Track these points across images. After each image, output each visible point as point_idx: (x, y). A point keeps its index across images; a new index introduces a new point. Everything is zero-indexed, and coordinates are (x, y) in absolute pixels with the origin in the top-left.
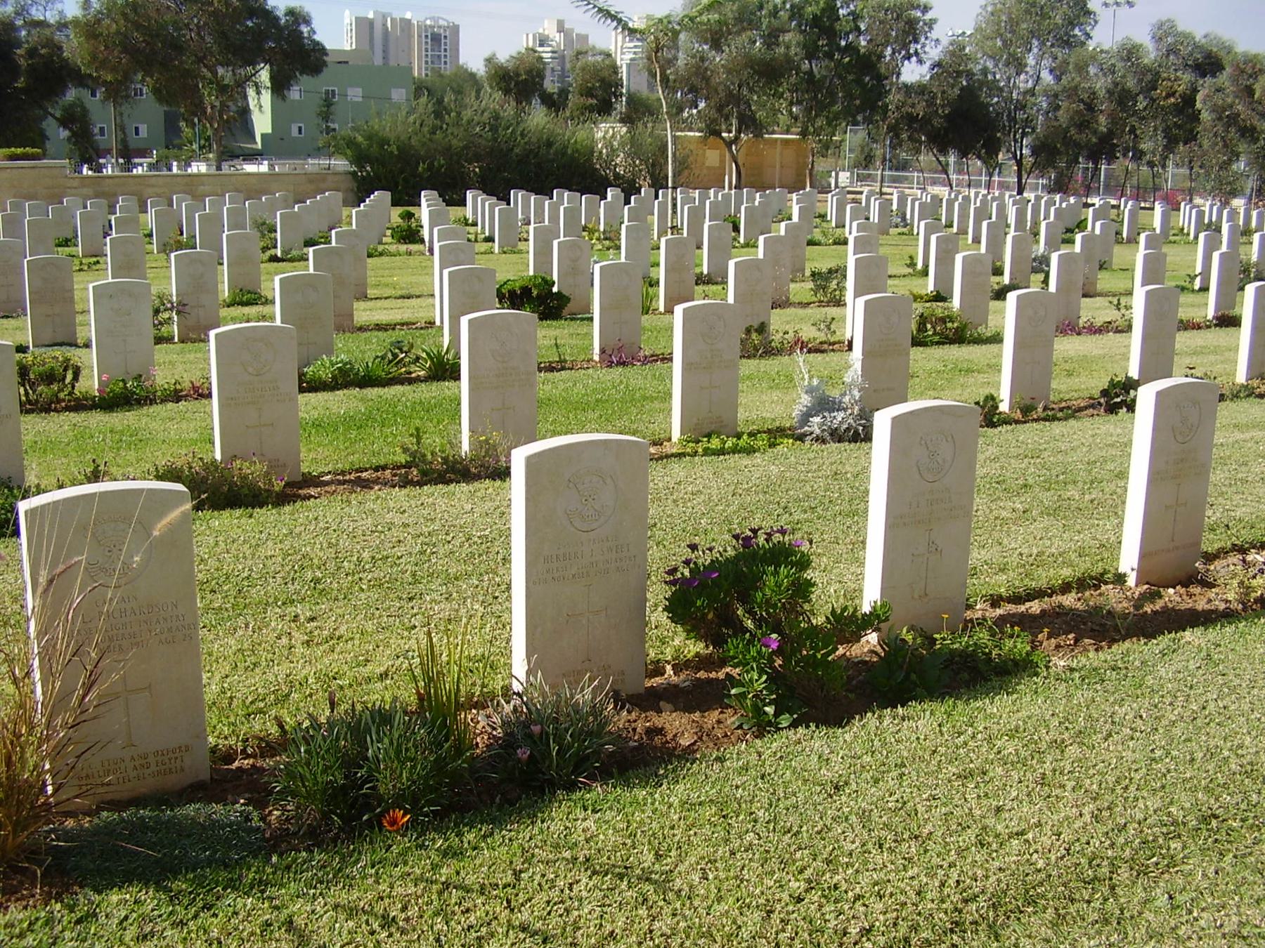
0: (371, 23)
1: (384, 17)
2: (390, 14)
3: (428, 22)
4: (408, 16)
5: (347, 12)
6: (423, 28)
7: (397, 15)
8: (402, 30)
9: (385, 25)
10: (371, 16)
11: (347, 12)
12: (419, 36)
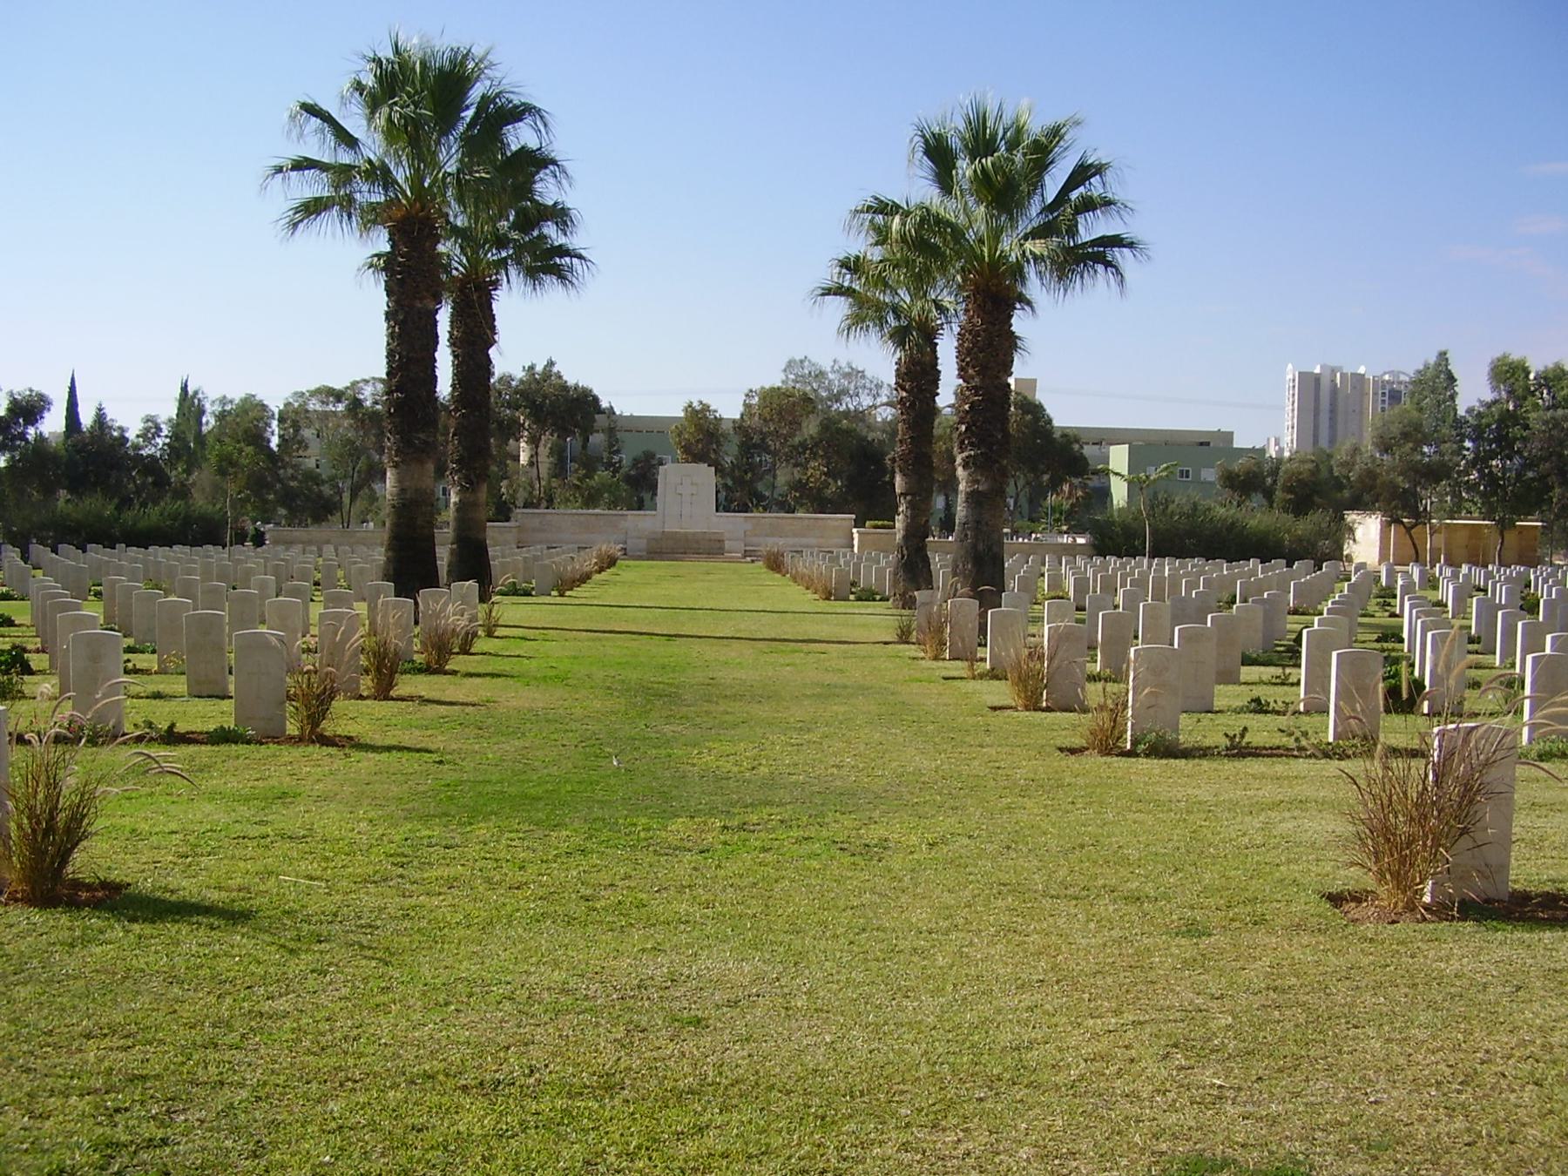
0: (1317, 379)
1: (1333, 371)
2: (1340, 369)
3: (1387, 377)
4: (1362, 370)
5: (1290, 366)
6: (1380, 384)
7: (1348, 370)
8: (1354, 388)
9: (1333, 381)
10: (1317, 370)
11: (1290, 366)
12: (1375, 394)
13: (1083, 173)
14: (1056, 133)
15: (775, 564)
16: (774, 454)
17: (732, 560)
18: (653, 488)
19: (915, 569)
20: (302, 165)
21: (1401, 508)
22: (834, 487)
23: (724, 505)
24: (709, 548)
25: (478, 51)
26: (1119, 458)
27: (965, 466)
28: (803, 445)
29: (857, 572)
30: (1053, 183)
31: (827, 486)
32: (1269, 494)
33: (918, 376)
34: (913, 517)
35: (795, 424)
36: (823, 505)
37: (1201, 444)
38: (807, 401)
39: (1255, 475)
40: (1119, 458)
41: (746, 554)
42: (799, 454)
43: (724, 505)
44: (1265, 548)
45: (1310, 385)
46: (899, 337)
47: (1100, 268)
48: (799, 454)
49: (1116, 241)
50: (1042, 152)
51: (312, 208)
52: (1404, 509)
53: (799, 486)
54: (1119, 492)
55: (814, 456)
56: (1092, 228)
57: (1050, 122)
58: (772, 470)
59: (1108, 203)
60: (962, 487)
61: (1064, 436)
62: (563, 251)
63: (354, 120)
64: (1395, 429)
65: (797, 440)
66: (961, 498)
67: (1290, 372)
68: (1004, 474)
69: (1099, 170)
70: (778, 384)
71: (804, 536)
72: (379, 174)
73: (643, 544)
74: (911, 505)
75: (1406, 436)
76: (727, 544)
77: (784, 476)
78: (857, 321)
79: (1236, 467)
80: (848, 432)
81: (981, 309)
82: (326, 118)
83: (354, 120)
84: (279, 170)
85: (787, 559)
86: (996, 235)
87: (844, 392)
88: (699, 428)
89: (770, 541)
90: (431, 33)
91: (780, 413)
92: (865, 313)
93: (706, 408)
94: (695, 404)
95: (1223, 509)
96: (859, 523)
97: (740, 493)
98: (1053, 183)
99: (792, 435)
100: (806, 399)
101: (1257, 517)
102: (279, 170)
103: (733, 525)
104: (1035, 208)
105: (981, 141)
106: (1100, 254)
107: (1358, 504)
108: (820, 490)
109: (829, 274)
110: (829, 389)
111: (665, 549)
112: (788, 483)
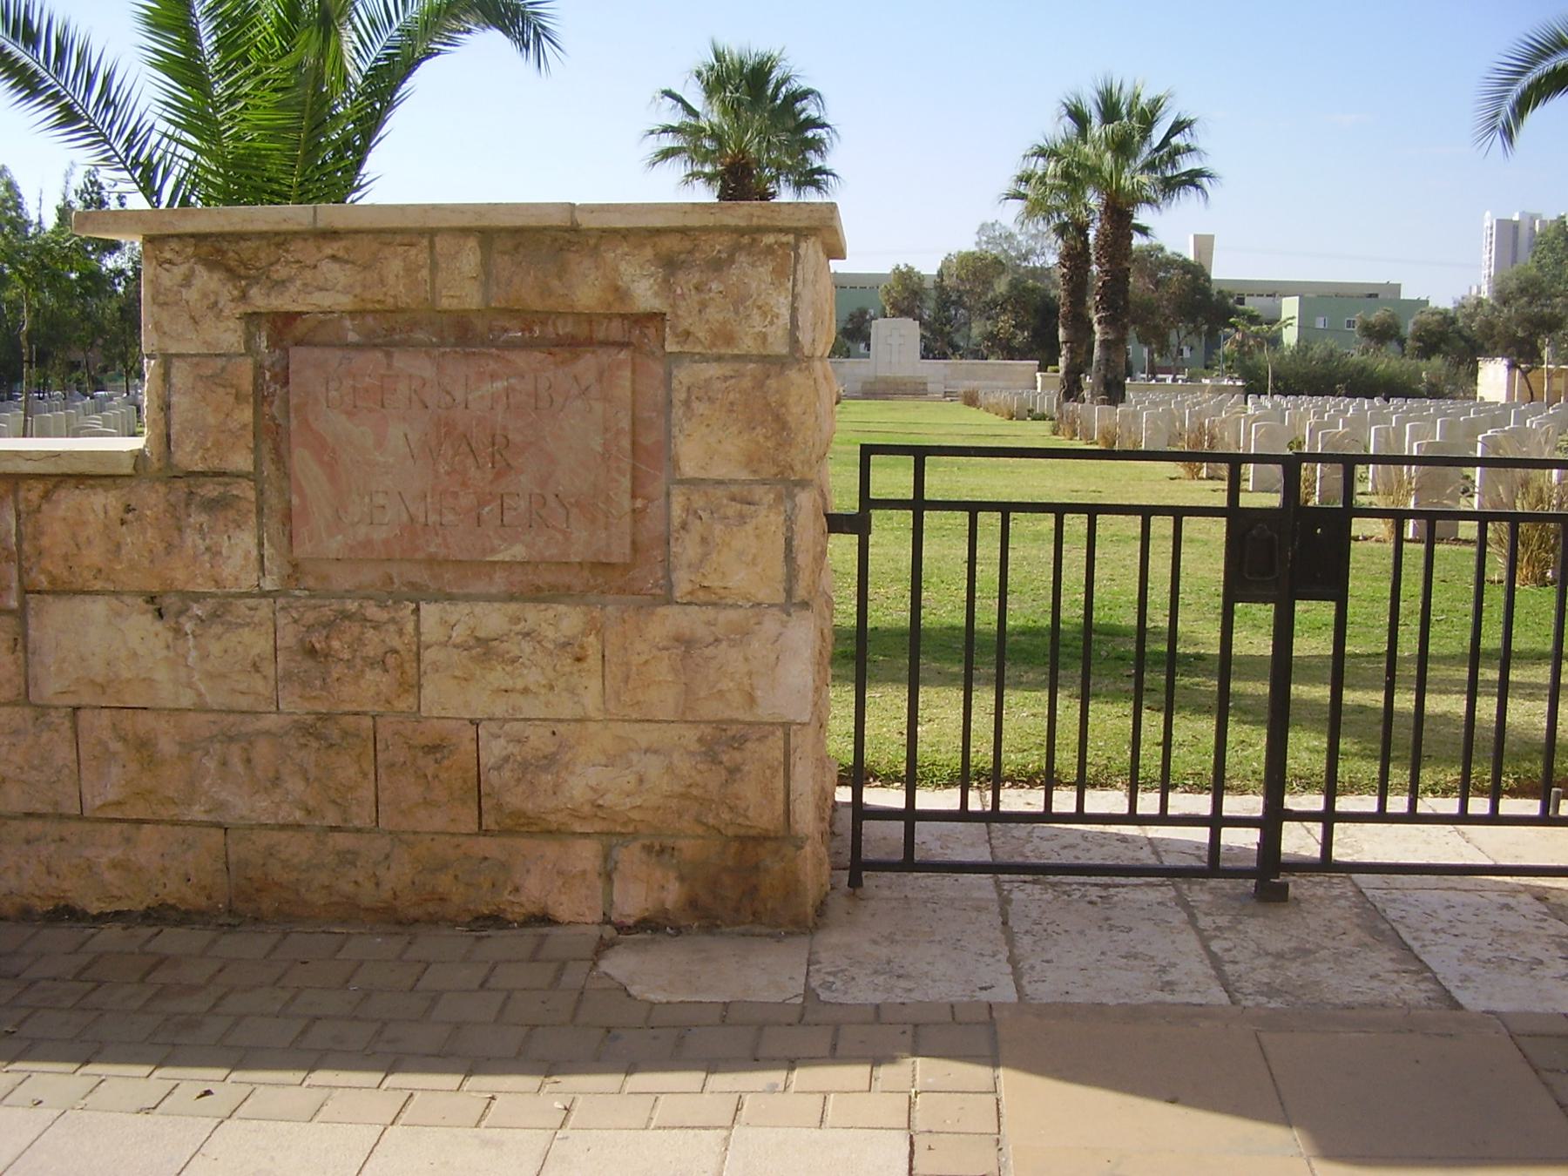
1: (1532, 219)
2: (1539, 216)
5: (1488, 214)
9: (1532, 229)
10: (1516, 218)
11: (1488, 214)
13: (1178, 127)
14: (1156, 104)
15: (971, 400)
16: (969, 309)
17: (934, 400)
18: (866, 339)
19: (1072, 390)
20: (666, 130)
21: (1523, 354)
22: (1022, 337)
23: (927, 353)
24: (916, 390)
25: (776, 54)
26: (1290, 307)
27: (1099, 323)
28: (995, 303)
29: (1034, 403)
30: (1158, 135)
31: (1014, 336)
32: (1402, 342)
33: (1075, 259)
34: (1072, 359)
35: (987, 284)
36: (1011, 352)
37: (1370, 296)
38: (998, 265)
39: (1390, 326)
40: (1290, 307)
41: (946, 395)
42: (991, 308)
43: (927, 353)
44: (1392, 388)
45: (1508, 232)
46: (1061, 230)
47: (1192, 189)
48: (991, 308)
49: (1199, 173)
50: (1148, 119)
51: (667, 154)
52: (1520, 356)
53: (991, 337)
54: (1290, 336)
55: (1004, 311)
56: (1186, 164)
57: (1153, 96)
58: (968, 323)
59: (1189, 149)
60: (1097, 336)
61: (1220, 292)
62: (820, 171)
63: (696, 98)
64: (1513, 285)
65: (990, 295)
66: (1097, 344)
67: (1488, 220)
68: (1125, 328)
69: (1189, 124)
70: (974, 248)
71: (994, 379)
72: (716, 136)
73: (859, 386)
74: (1071, 350)
75: (1522, 291)
76: (930, 387)
77: (977, 329)
78: (1030, 213)
79: (1372, 319)
80: (1034, 290)
81: (1110, 220)
82: (679, 99)
83: (696, 98)
84: (652, 132)
85: (981, 395)
86: (1120, 172)
87: (1031, 251)
88: (905, 287)
89: (967, 383)
90: (746, 43)
91: (974, 274)
92: (1037, 208)
93: (911, 269)
94: (902, 267)
95: (1356, 353)
96: (1042, 368)
97: (938, 344)
98: (1158, 135)
99: (985, 294)
100: (997, 261)
101: (1386, 361)
102: (652, 132)
103: (934, 370)
104: (1146, 150)
105: (1110, 110)
106: (1193, 179)
107: (1491, 354)
108: (1009, 340)
109: (1008, 185)
110: (1018, 250)
111: (877, 391)
112: (981, 334)
